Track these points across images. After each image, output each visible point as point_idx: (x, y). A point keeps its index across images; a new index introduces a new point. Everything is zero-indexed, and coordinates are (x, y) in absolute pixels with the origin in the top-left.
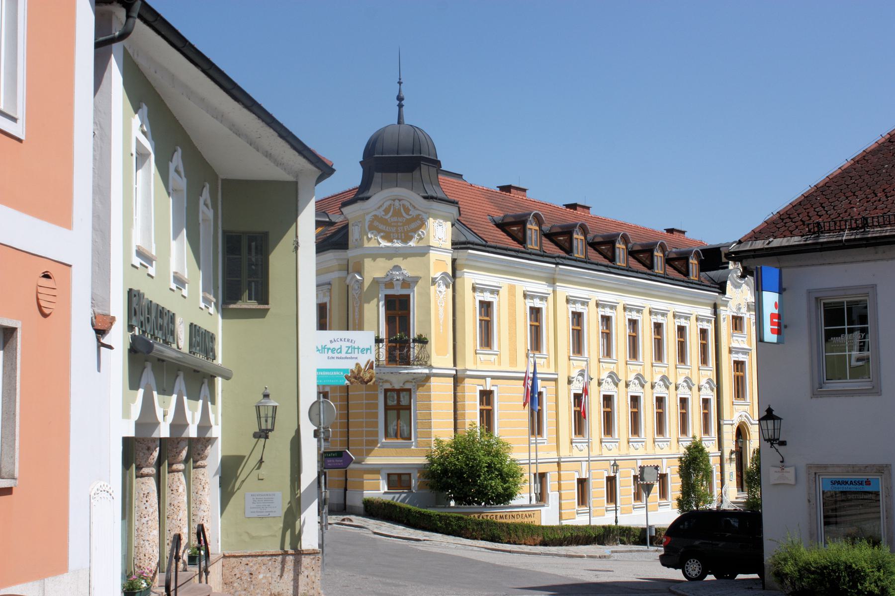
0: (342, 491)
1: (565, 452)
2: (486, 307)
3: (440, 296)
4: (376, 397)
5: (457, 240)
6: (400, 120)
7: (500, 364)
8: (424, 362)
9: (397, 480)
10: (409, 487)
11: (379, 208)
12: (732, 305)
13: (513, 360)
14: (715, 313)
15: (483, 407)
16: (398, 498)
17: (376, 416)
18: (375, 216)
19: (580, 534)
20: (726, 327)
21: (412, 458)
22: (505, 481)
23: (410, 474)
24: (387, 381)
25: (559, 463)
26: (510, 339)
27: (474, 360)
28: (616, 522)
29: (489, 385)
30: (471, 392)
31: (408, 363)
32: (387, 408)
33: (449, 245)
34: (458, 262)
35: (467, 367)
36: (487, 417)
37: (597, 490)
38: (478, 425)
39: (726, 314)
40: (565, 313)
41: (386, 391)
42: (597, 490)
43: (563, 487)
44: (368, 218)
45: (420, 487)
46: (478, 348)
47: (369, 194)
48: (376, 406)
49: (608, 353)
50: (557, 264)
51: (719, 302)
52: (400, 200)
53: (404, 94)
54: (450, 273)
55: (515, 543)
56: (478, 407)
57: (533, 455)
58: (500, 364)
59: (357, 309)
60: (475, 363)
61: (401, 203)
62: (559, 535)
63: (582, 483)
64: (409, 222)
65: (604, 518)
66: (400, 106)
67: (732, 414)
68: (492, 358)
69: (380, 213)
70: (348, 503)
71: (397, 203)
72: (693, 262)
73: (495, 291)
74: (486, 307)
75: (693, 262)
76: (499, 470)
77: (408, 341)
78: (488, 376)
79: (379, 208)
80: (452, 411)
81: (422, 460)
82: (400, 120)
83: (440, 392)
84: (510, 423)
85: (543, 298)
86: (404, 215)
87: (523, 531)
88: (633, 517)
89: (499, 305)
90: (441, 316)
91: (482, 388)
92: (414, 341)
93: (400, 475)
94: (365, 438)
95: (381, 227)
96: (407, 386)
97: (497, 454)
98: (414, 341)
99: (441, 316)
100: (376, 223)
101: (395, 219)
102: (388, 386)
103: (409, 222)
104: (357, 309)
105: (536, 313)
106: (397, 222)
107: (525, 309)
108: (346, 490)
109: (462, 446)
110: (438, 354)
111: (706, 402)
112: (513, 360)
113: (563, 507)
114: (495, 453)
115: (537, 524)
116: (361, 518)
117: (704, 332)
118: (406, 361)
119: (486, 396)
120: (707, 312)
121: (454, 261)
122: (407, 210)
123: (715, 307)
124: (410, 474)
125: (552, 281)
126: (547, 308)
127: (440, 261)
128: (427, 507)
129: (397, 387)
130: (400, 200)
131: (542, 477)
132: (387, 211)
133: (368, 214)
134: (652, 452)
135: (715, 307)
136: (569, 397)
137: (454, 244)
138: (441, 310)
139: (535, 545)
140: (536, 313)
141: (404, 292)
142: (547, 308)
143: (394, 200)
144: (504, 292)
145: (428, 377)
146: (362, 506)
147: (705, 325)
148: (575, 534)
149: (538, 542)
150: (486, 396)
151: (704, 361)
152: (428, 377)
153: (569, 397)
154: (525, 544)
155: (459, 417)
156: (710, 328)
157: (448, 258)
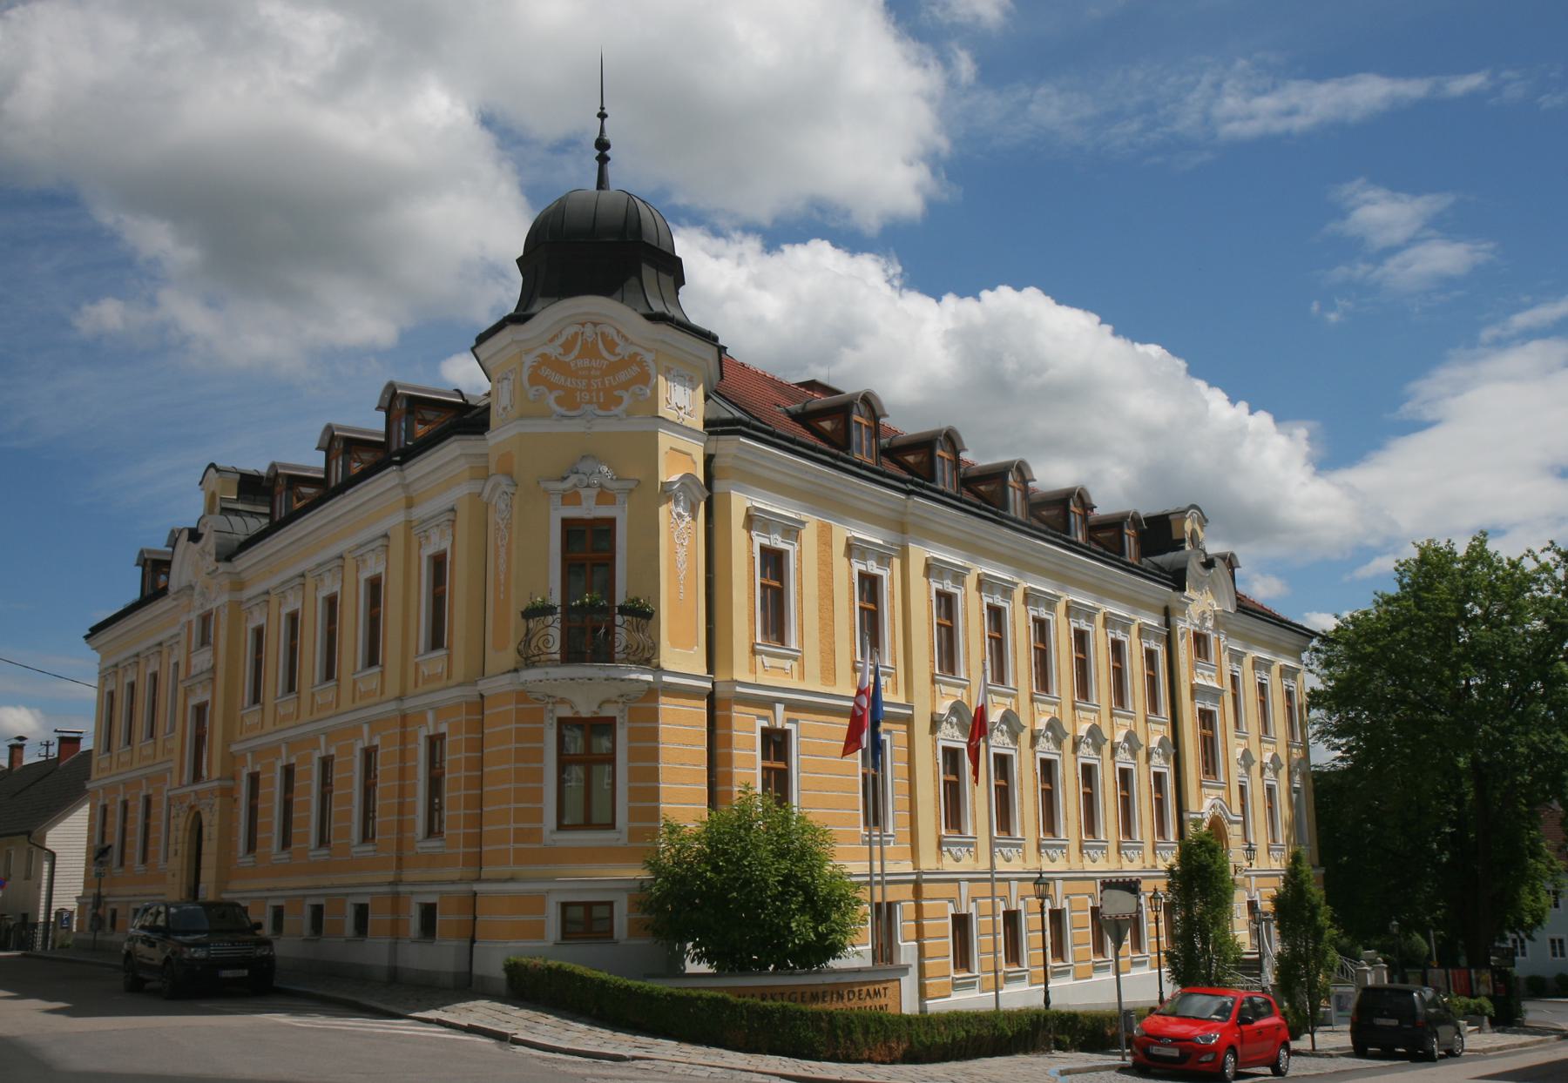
0: (467, 944)
1: (928, 862)
2: (774, 561)
3: (678, 537)
4: (539, 736)
5: (713, 416)
6: (602, 183)
7: (802, 676)
8: (647, 656)
9: (584, 922)
10: (608, 934)
11: (551, 340)
12: (1194, 610)
13: (829, 672)
14: (1168, 624)
15: (768, 764)
16: (580, 961)
17: (538, 775)
18: (543, 356)
19: (985, 1032)
20: (1184, 649)
21: (617, 876)
22: (820, 916)
23: (610, 904)
24: (563, 701)
25: (917, 886)
26: (822, 630)
27: (748, 668)
28: (1047, 1001)
29: (781, 718)
30: (747, 729)
31: (610, 658)
32: (564, 763)
33: (700, 426)
34: (717, 462)
35: (737, 677)
36: (778, 781)
37: (986, 939)
38: (759, 790)
39: (1185, 626)
40: (923, 594)
41: (562, 722)
42: (986, 939)
43: (927, 933)
44: (529, 360)
45: (635, 928)
46: (759, 640)
47: (533, 310)
48: (539, 755)
49: (1000, 677)
50: (909, 493)
51: (1173, 605)
52: (595, 324)
53: (608, 136)
54: (701, 476)
55: (847, 1059)
56: (759, 763)
57: (877, 870)
58: (802, 676)
59: (503, 551)
60: (753, 671)
61: (598, 329)
62: (943, 1038)
63: (961, 923)
64: (614, 368)
65: (1020, 996)
66: (603, 160)
67: (1201, 804)
68: (787, 664)
69: (554, 350)
70: (477, 970)
71: (589, 330)
72: (1129, 534)
73: (792, 530)
74: (774, 561)
75: (1129, 534)
76: (804, 887)
77: (608, 611)
78: (780, 700)
79: (551, 340)
80: (704, 768)
81: (639, 873)
82: (602, 183)
83: (680, 727)
84: (825, 785)
85: (884, 560)
86: (605, 354)
87: (866, 1032)
88: (1084, 988)
89: (800, 560)
90: (683, 568)
91: (765, 724)
92: (623, 610)
93: (588, 906)
94: (513, 826)
95: (556, 378)
96: (608, 712)
97: (803, 854)
98: (623, 610)
99: (683, 568)
100: (545, 371)
101: (586, 363)
102: (565, 712)
103: (614, 368)
104: (503, 551)
105: (870, 586)
106: (589, 369)
107: (851, 574)
108: (473, 941)
109: (726, 843)
110: (674, 644)
111: (1159, 777)
112: (829, 672)
113: (928, 973)
114: (798, 853)
115: (892, 1010)
116: (498, 1005)
117: (1150, 655)
118: (603, 652)
119: (776, 743)
120: (1153, 621)
121: (709, 460)
122: (611, 346)
123: (1167, 614)
124: (610, 904)
125: (902, 527)
126: (892, 578)
127: (680, 456)
128: (647, 976)
129: (585, 712)
130: (595, 324)
131: (884, 914)
132: (568, 347)
133: (527, 352)
134: (1078, 867)
135: (1167, 614)
136: (935, 754)
137: (708, 423)
138: (682, 552)
139: (892, 1062)
140: (870, 586)
141: (603, 512)
142: (892, 578)
143: (583, 325)
144: (809, 535)
145: (652, 693)
146: (504, 975)
147: (1153, 645)
148: (974, 1032)
149: (898, 1053)
150: (776, 743)
151: (1154, 706)
152: (652, 693)
153: (935, 754)
154: (870, 1060)
155: (719, 722)
156: (1161, 650)
157: (697, 450)
